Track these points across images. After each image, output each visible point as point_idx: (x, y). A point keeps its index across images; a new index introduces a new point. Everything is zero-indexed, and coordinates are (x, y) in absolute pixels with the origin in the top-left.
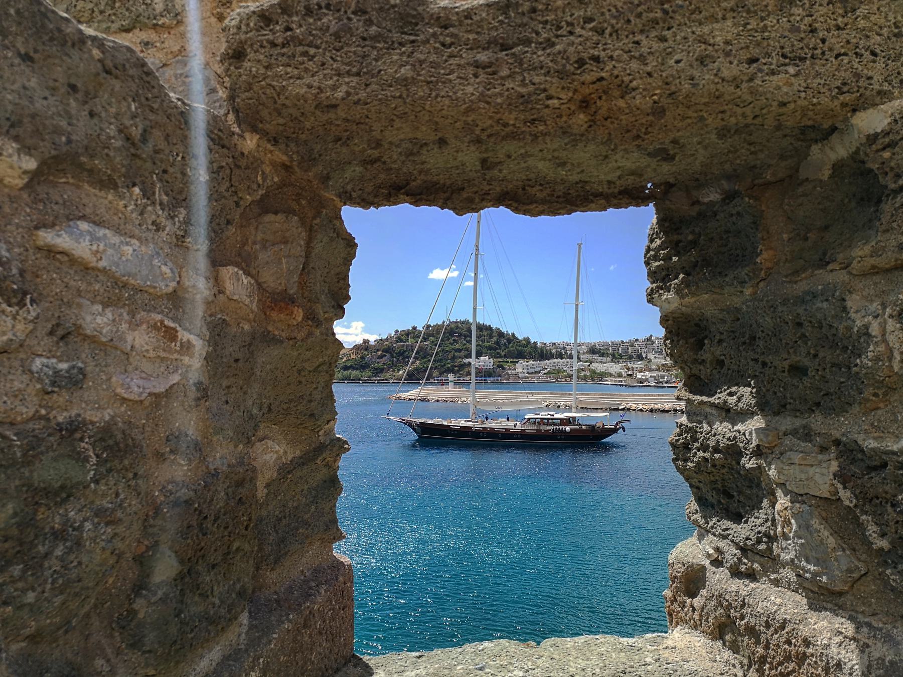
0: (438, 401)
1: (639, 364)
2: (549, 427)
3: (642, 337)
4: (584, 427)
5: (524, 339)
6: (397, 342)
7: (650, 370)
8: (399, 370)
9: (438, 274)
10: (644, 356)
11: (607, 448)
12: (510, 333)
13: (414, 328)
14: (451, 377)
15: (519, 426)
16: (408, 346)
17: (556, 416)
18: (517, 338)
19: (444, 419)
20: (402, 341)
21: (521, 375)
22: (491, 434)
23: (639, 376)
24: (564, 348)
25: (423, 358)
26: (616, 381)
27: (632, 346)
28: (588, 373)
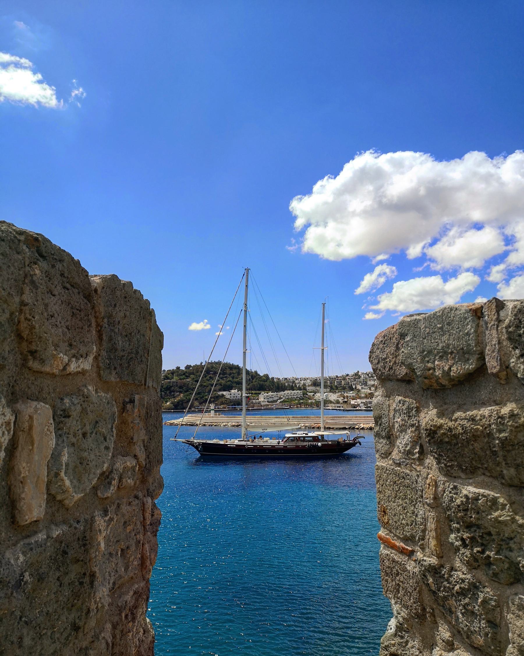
0: (204, 425)
1: (351, 394)
2: (305, 444)
3: (351, 373)
4: (330, 443)
5: (264, 376)
6: (165, 379)
7: (360, 398)
8: (167, 402)
9: (195, 326)
10: (354, 387)
11: (349, 458)
12: (253, 371)
13: (178, 368)
14: (212, 406)
15: (282, 444)
16: (174, 382)
17: (310, 435)
18: (259, 375)
19: (221, 440)
20: (168, 378)
21: (262, 404)
22: (261, 450)
23: (353, 402)
24: (294, 382)
25: (186, 392)
26: (335, 407)
27: (344, 379)
28: (314, 401)
